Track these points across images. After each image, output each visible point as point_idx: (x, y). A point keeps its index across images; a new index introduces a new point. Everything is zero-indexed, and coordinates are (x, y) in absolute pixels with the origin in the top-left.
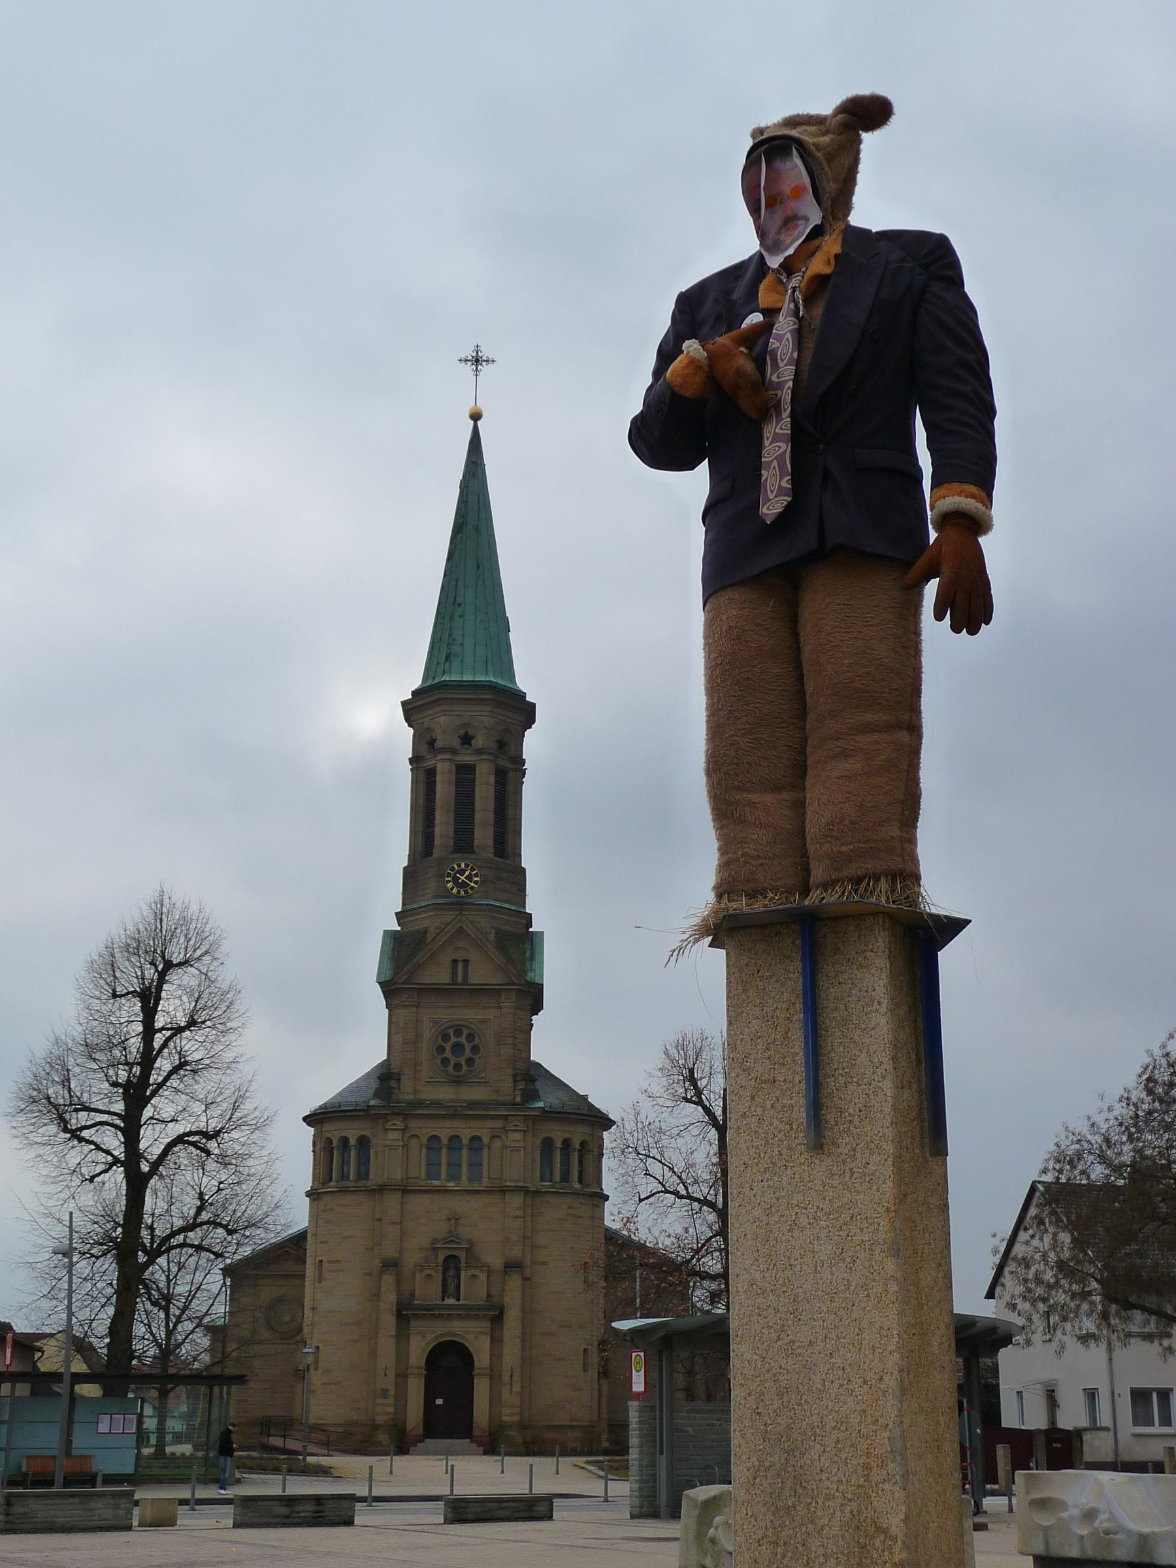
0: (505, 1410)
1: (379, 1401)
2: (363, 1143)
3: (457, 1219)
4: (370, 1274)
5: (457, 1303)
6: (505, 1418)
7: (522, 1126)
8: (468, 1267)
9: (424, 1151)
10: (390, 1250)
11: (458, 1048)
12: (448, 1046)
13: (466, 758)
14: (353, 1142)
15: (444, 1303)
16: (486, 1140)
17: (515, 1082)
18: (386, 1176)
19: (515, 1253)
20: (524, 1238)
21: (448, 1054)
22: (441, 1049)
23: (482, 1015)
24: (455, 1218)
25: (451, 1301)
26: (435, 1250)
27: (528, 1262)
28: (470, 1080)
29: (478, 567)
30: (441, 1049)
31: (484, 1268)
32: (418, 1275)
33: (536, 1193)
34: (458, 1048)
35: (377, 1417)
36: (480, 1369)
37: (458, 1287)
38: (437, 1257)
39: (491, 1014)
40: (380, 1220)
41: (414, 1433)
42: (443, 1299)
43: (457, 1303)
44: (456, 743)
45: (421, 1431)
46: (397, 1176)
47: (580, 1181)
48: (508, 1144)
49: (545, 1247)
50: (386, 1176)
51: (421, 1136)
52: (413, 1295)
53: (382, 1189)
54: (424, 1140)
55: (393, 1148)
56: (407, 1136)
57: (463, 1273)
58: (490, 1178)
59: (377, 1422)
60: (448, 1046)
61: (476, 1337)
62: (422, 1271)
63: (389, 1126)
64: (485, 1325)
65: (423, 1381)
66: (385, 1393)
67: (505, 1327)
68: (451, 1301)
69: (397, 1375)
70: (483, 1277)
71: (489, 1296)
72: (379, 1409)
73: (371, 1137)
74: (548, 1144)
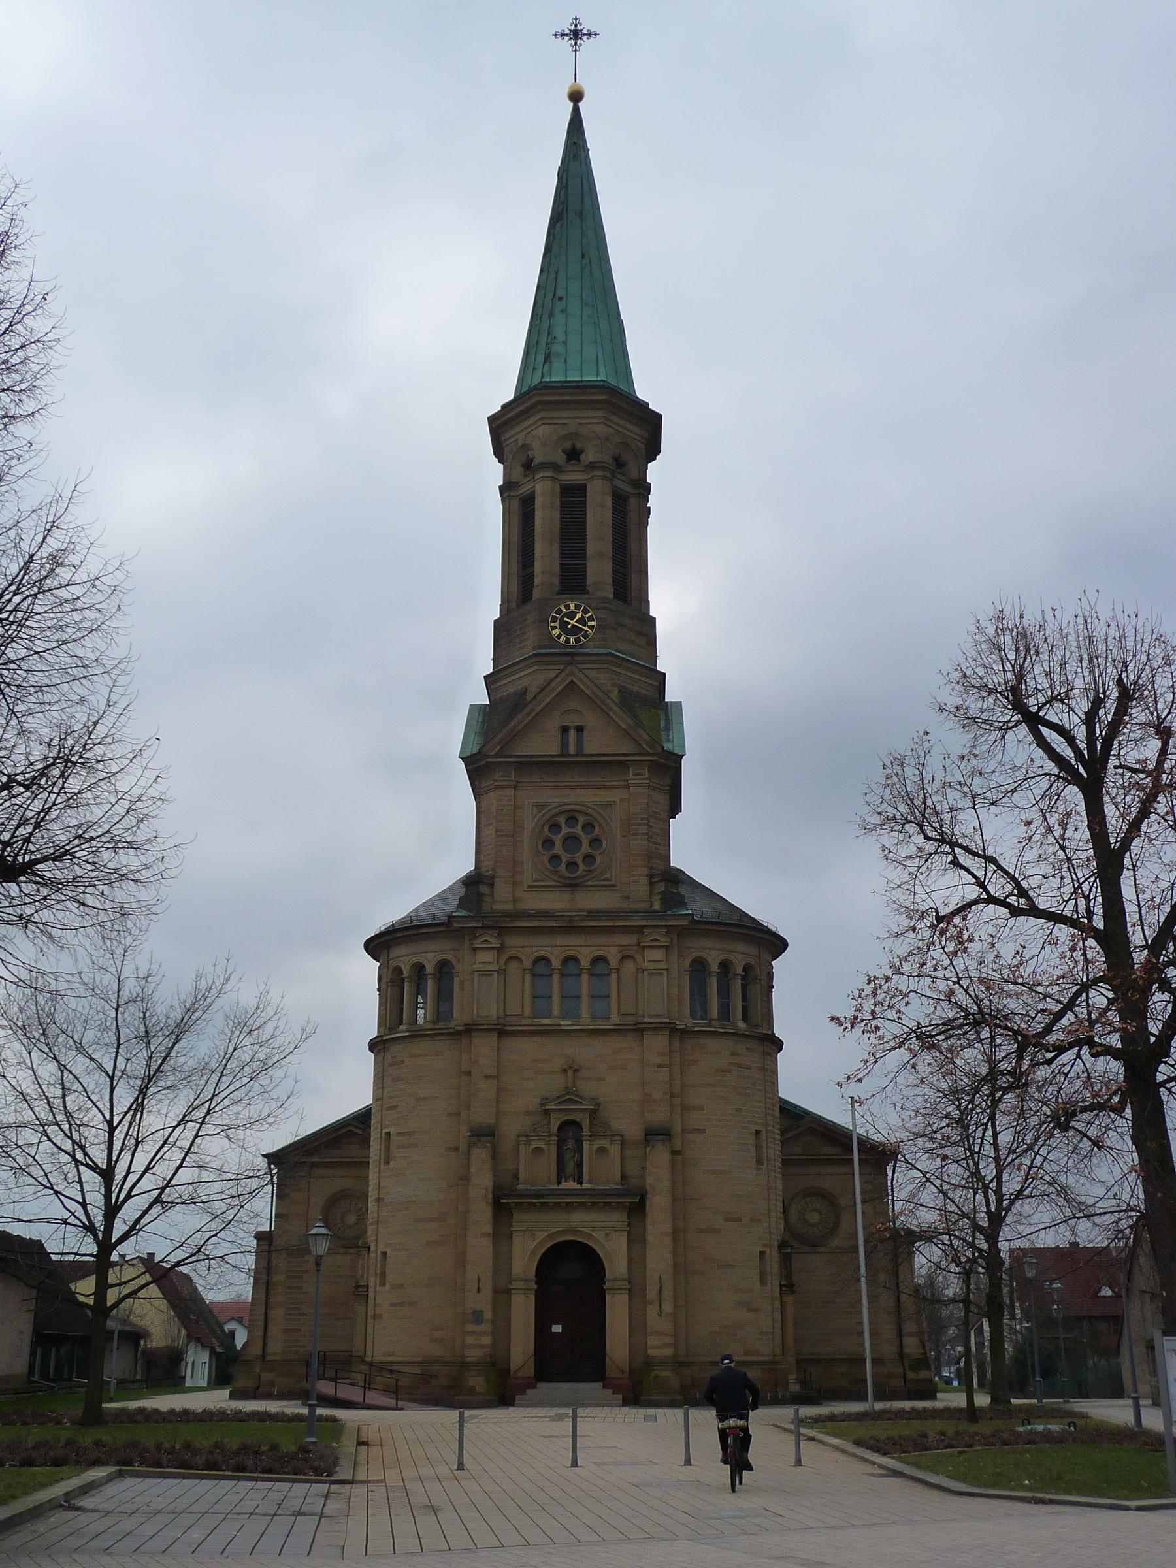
0: (652, 1341)
1: (470, 1327)
2: (444, 970)
3: (576, 1071)
4: (456, 1149)
5: (579, 1187)
6: (651, 1352)
7: (664, 941)
8: (593, 1136)
9: (528, 977)
10: (482, 1115)
11: (571, 841)
12: (558, 839)
13: (574, 476)
14: (429, 969)
15: (561, 1187)
16: (614, 962)
17: (651, 884)
18: (475, 1012)
19: (659, 1116)
20: (672, 1096)
21: (558, 849)
22: (548, 843)
23: (603, 796)
24: (573, 1069)
25: (571, 1185)
26: (547, 1113)
27: (677, 1129)
28: (590, 883)
29: (583, 256)
30: (548, 843)
31: (616, 1138)
32: (522, 1148)
33: (685, 1033)
34: (571, 841)
35: (467, 1352)
36: (614, 1280)
37: (579, 1165)
38: (549, 1123)
39: (616, 796)
40: (469, 1073)
41: (520, 1374)
42: (559, 1183)
43: (579, 1187)
44: (560, 458)
45: (530, 1371)
46: (491, 1011)
47: (745, 1018)
48: (646, 965)
49: (701, 1109)
50: (475, 1012)
51: (523, 958)
52: (516, 1177)
53: (469, 1030)
54: (528, 964)
55: (485, 974)
56: (504, 958)
57: (586, 1145)
58: (620, 1014)
59: (468, 1360)
60: (558, 839)
61: (607, 1235)
62: (528, 1143)
63: (478, 943)
64: (619, 1218)
65: (533, 1298)
66: (478, 1317)
67: (649, 1221)
68: (571, 1185)
69: (496, 1291)
70: (614, 1149)
71: (624, 1177)
72: (470, 1340)
73: (454, 961)
74: (699, 967)
